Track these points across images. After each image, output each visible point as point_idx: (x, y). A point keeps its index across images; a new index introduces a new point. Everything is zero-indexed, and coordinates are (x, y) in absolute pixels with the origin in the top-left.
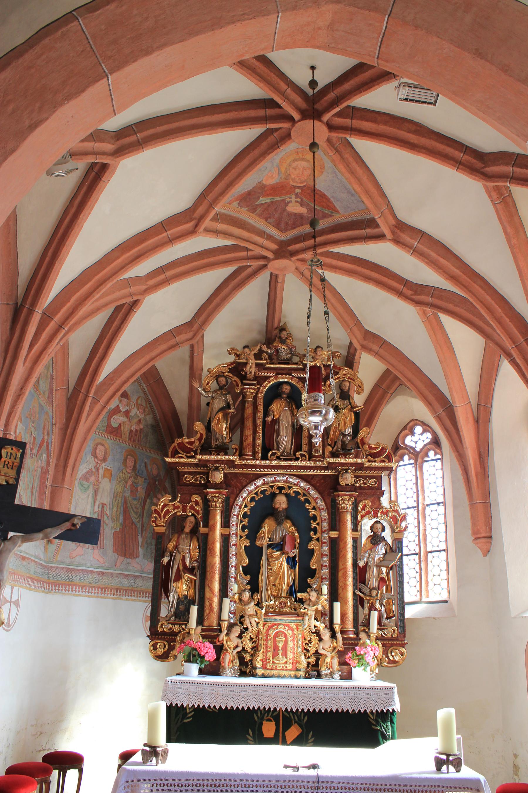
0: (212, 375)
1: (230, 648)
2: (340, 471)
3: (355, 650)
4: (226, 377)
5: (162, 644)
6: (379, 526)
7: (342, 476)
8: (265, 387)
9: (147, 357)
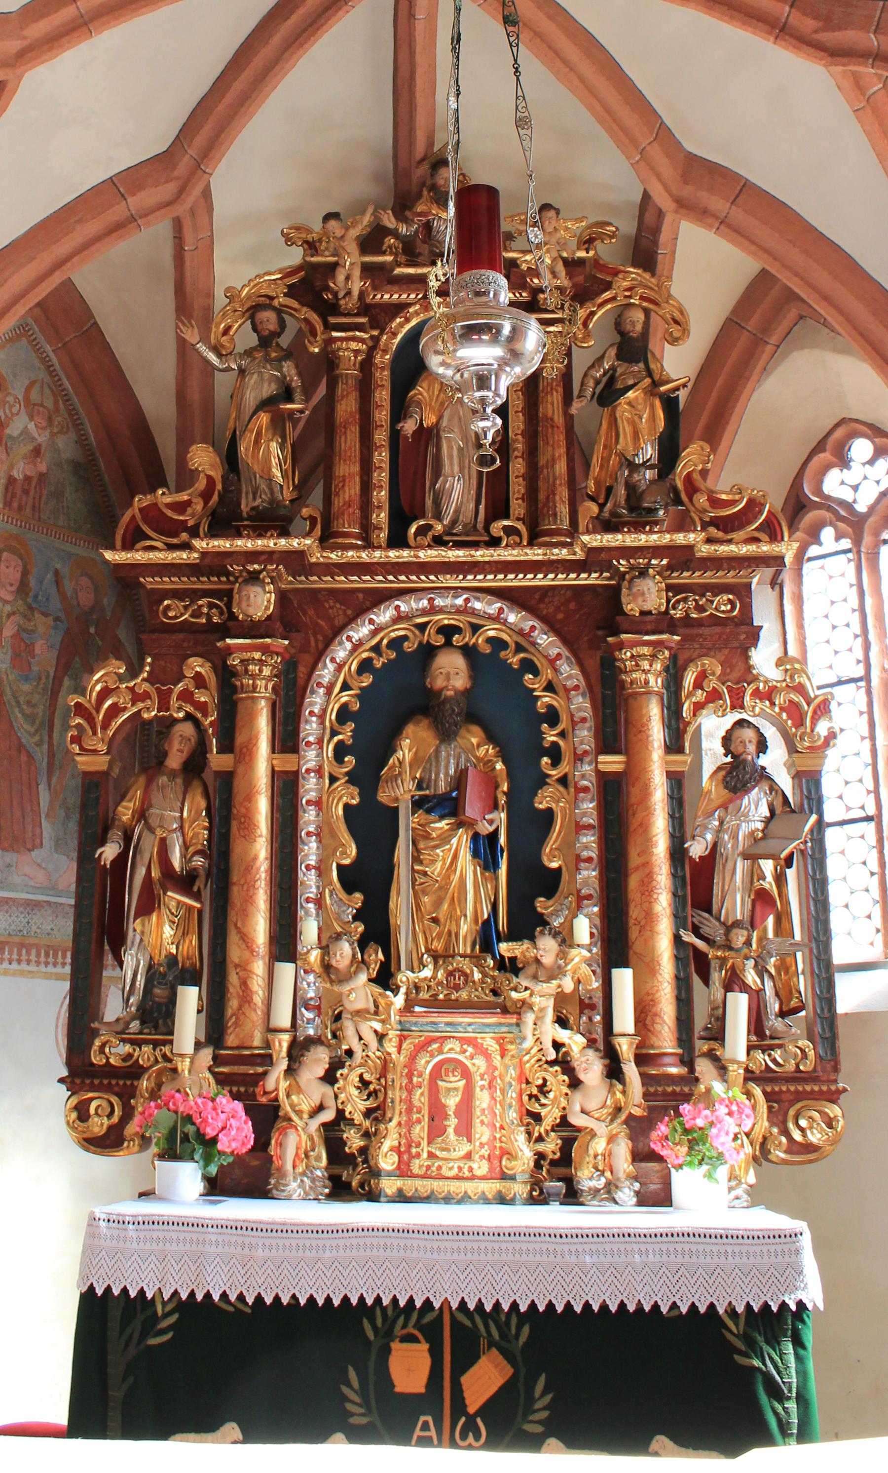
0: (237, 306)
1: (299, 1113)
2: (625, 573)
3: (678, 1114)
4: (279, 311)
5: (105, 1104)
6: (748, 734)
7: (629, 588)
8: (395, 334)
9: (45, 260)
